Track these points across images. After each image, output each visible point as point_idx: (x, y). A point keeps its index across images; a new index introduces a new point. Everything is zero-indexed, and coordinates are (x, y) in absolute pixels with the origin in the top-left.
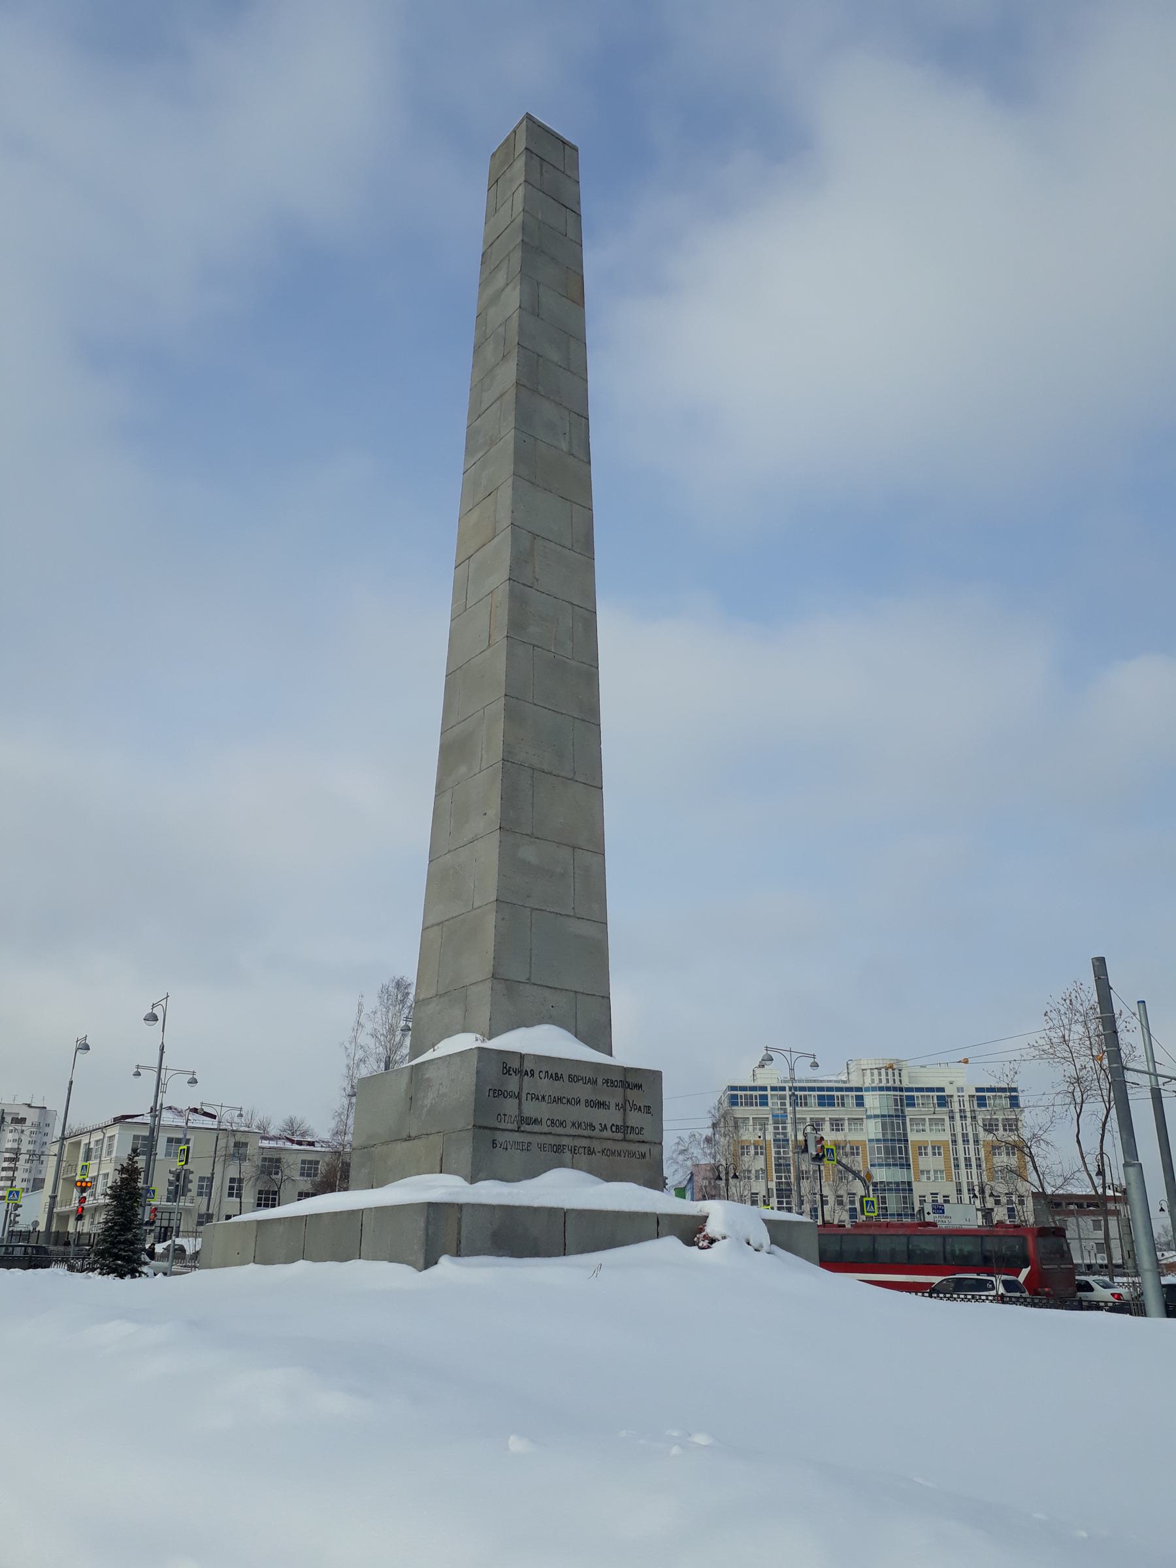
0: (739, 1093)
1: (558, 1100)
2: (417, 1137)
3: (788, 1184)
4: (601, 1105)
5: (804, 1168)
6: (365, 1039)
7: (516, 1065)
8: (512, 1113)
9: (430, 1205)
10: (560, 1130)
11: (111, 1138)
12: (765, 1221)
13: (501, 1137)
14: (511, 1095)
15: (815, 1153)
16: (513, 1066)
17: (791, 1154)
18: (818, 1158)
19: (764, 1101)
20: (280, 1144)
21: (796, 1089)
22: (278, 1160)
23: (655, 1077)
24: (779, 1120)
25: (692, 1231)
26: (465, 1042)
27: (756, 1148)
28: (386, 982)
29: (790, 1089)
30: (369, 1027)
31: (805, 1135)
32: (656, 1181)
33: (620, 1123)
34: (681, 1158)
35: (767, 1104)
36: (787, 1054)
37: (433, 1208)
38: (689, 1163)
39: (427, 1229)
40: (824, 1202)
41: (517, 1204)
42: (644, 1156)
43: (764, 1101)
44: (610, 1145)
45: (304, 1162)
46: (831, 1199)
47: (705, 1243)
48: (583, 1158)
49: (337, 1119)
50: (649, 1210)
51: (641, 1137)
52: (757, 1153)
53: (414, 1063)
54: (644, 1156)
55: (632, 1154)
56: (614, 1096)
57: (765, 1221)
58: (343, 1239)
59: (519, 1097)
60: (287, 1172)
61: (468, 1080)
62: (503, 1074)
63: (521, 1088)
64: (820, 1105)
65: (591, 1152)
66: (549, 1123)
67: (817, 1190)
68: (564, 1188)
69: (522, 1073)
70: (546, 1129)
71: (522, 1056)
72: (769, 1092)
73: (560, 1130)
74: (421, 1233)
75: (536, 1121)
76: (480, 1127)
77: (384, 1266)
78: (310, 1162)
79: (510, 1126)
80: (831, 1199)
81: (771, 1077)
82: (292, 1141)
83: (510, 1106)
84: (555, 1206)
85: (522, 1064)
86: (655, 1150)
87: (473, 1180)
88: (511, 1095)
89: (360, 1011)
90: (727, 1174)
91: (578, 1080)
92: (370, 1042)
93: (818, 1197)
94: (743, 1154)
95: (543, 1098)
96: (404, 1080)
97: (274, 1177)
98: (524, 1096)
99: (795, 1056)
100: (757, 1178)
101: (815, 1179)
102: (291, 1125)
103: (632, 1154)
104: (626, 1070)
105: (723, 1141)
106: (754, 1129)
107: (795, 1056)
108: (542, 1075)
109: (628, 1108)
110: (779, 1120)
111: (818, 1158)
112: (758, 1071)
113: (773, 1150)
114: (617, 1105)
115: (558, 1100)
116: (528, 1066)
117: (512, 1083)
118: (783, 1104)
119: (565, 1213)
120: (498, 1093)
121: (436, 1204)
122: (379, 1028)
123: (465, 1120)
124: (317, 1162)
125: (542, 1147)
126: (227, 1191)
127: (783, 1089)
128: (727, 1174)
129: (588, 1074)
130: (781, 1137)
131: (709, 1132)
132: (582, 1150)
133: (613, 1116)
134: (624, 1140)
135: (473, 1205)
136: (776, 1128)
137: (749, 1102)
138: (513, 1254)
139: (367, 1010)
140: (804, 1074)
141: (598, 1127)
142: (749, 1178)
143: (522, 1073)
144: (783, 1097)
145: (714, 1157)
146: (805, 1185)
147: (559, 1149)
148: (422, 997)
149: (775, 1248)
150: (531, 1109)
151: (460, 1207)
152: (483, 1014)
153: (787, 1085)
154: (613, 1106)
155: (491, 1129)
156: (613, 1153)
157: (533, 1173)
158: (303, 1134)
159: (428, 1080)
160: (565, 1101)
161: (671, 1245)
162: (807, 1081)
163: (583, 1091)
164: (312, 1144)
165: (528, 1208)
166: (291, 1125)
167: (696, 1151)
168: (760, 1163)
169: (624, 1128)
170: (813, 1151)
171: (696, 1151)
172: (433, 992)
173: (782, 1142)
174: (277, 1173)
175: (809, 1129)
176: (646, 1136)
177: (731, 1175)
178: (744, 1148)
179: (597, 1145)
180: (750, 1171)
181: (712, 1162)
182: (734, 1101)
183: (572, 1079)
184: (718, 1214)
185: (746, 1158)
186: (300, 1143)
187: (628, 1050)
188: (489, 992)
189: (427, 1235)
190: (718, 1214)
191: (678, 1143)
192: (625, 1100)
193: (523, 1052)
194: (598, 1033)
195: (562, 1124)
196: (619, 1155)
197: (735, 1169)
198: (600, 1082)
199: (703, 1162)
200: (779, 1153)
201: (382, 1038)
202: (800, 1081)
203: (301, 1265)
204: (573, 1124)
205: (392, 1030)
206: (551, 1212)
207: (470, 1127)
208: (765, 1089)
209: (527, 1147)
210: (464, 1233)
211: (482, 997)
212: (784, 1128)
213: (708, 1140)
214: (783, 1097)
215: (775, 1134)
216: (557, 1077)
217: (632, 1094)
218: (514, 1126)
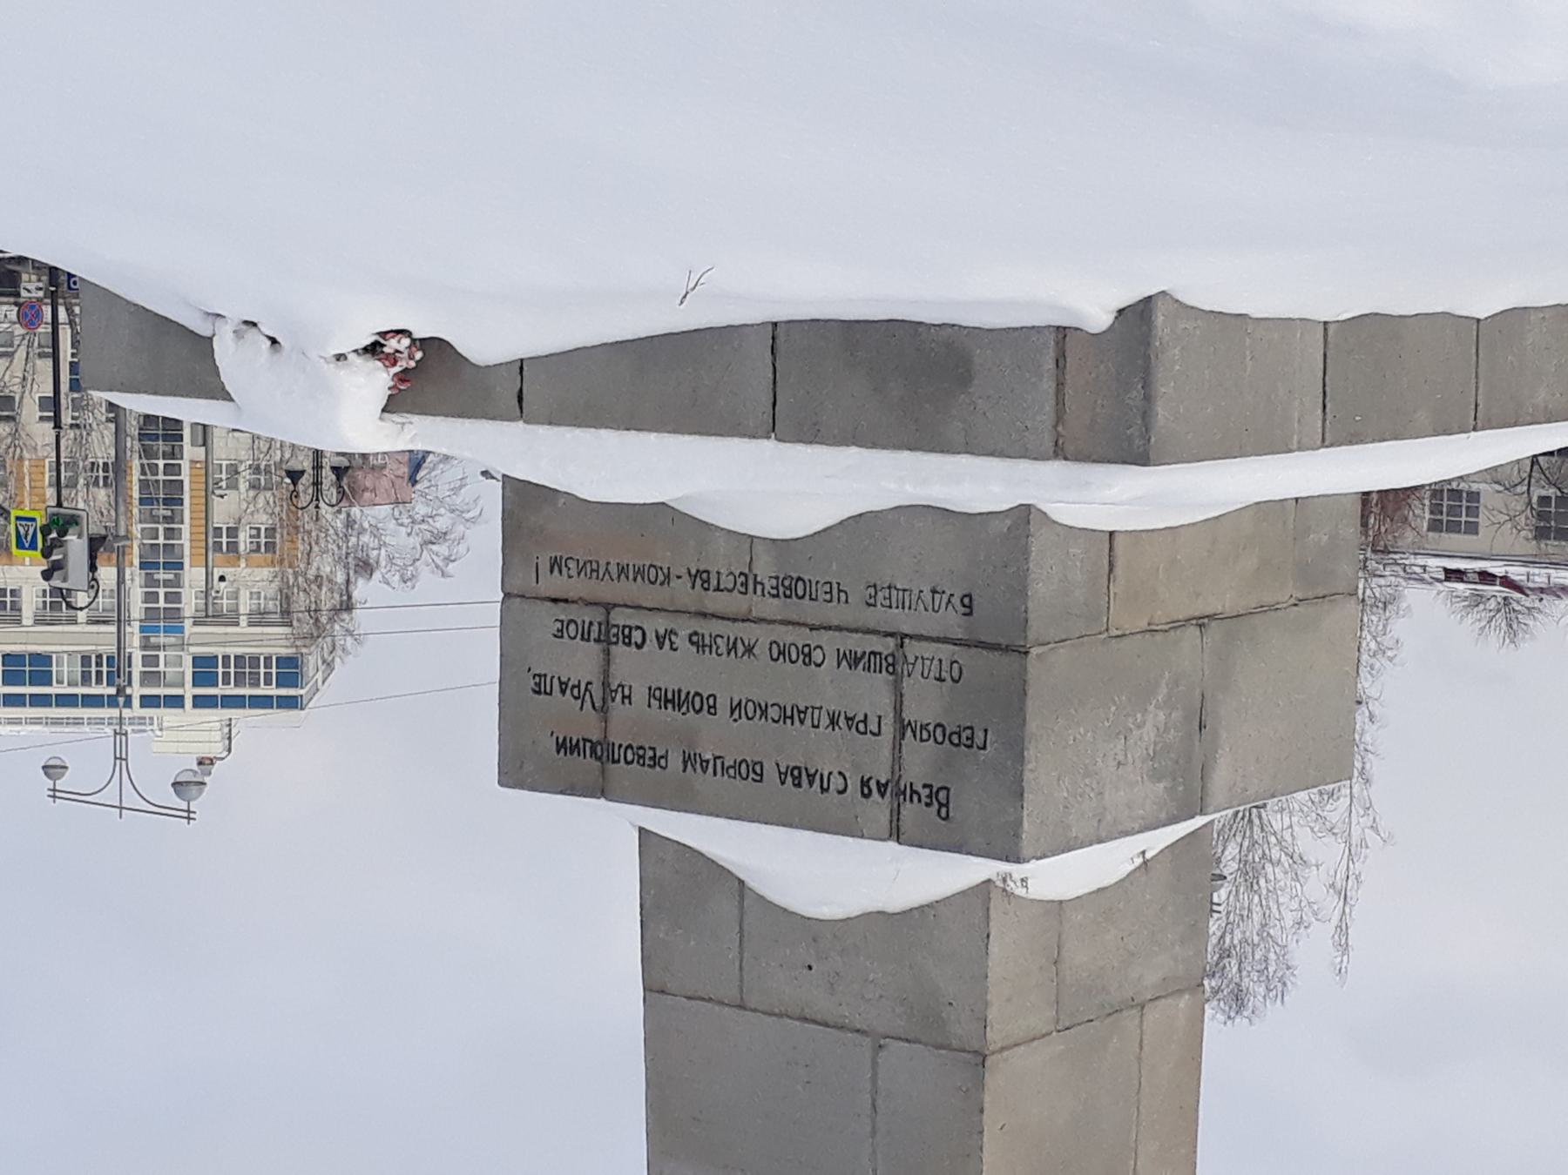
0: (273, 691)
1: (793, 715)
2: (1178, 625)
3: (147, 453)
4: (672, 700)
5: (102, 494)
6: (1324, 853)
7: (909, 810)
8: (927, 686)
9: (1143, 459)
10: (788, 635)
12: (228, 397)
13: (951, 621)
14: (923, 732)
15: (71, 537)
16: (917, 808)
17: (136, 529)
18: (62, 523)
19: (205, 670)
20: (1540, 576)
21: (112, 702)
22: (1541, 534)
23: (517, 771)
24: (163, 619)
25: (427, 374)
26: (1056, 877)
27: (233, 547)
28: (1273, 1010)
29: (129, 699)
30: (1315, 886)
31: (93, 583)
32: (525, 504)
33: (619, 650)
34: (441, 524)
35: (196, 660)
36: (131, 799)
37: (1136, 451)
38: (421, 509)
39: (1148, 398)
40: (53, 404)
41: (906, 455)
42: (555, 564)
43: (205, 670)
44: (651, 595)
45: (1473, 529)
46: (30, 412)
47: (392, 345)
48: (722, 563)
49: (1387, 641)
50: (542, 430)
51: (562, 612)
52: (233, 532)
53: (1199, 821)
54: (555, 564)
55: (589, 569)
56: (633, 720)
57: (228, 397)
58: (1370, 370)
59: (902, 727)
60: (1518, 505)
61: (1045, 777)
62: (952, 779)
63: (897, 747)
64: (45, 659)
65: (701, 578)
66: (817, 656)
67: (68, 436)
68: (776, 490)
69: (895, 790)
70: (824, 638)
71: (896, 833)
72: (189, 691)
73: (788, 635)
74: (1165, 388)
75: (854, 660)
76: (1007, 649)
77: (1258, 306)
78: (1454, 527)
79: (927, 649)
80: (30, 412)
81: (185, 733)
82: (1507, 582)
83: (925, 703)
84: (800, 448)
85: (896, 814)
86: (520, 582)
87: (1024, 514)
88: (923, 732)
89: (1342, 929)
90: (317, 484)
91: (737, 766)
92: (1305, 841)
93: (66, 419)
94: (271, 531)
95: (833, 722)
96: (1221, 777)
97: (1551, 492)
98: (888, 728)
99: (110, 795)
100: (234, 471)
101: (73, 465)
102: (1512, 623)
103: (589, 569)
104: (601, 790)
105: (325, 565)
106: (235, 595)
108: (837, 782)
109: (597, 691)
110: (163, 619)
111: (62, 523)
112: (217, 749)
113: (185, 540)
114: (627, 698)
115: (793, 715)
116: (879, 808)
117: (920, 763)
118: (150, 661)
119: (772, 428)
120: (961, 738)
121: (1125, 462)
122: (1284, 880)
123: (1048, 670)
124: (1435, 526)
125: (836, 593)
127: (147, 701)
128: (317, 484)
129: (704, 782)
130: (162, 575)
131: (362, 589)
132: (727, 582)
133: (636, 668)
134: (609, 607)
135: (1025, 454)
136: (174, 597)
137: (246, 667)
138: (915, 328)
139: (1321, 934)
140: (83, 742)
141: (681, 641)
142: (256, 469)
143: (895, 790)
144: (149, 678)
145: (350, 523)
146: (101, 447)
147: (789, 587)
148: (1184, 1001)
149: (203, 329)
150: (869, 694)
151: (1059, 452)
152: (1006, 952)
153: (137, 710)
154: (640, 695)
155: (981, 645)
156: (639, 572)
157: (861, 529)
158: (1478, 600)
159: (1156, 776)
160: (773, 713)
161: (486, 342)
162: (78, 722)
163: (717, 735)
164: (1453, 575)
165: (874, 445)
166: (1512, 623)
167: (399, 539)
168: (224, 510)
169: (608, 637)
170: (76, 545)
171: (399, 539)
172: (1153, 1015)
173: (162, 562)
174: (1544, 500)
175: (82, 599)
176: (548, 617)
177: (306, 480)
178: (267, 545)
179: (683, 592)
180: (254, 486)
181: (355, 511)
182: (290, 671)
183: (755, 771)
184: (356, 416)
185: (263, 520)
186: (1486, 577)
187: (598, 841)
188: (992, 1014)
189: (1146, 384)
190: (356, 416)
191: (448, 560)
192: (603, 710)
193: (892, 845)
194: (678, 892)
195: (781, 653)
196: (623, 570)
197: (294, 494)
198: (675, 761)
199: (384, 510)
200: (170, 533)
201: (1275, 853)
202: (100, 721)
203: (1482, 306)
204: (749, 650)
205: (1250, 874)
206: (811, 432)
207: (1034, 651)
208: (200, 702)
209: (875, 593)
210: (1048, 385)
211: (1012, 1003)
212: (150, 597)
213: (366, 567)
214: (149, 678)
215: (177, 583)
216: (796, 776)
217: (586, 725)
218: (913, 649)
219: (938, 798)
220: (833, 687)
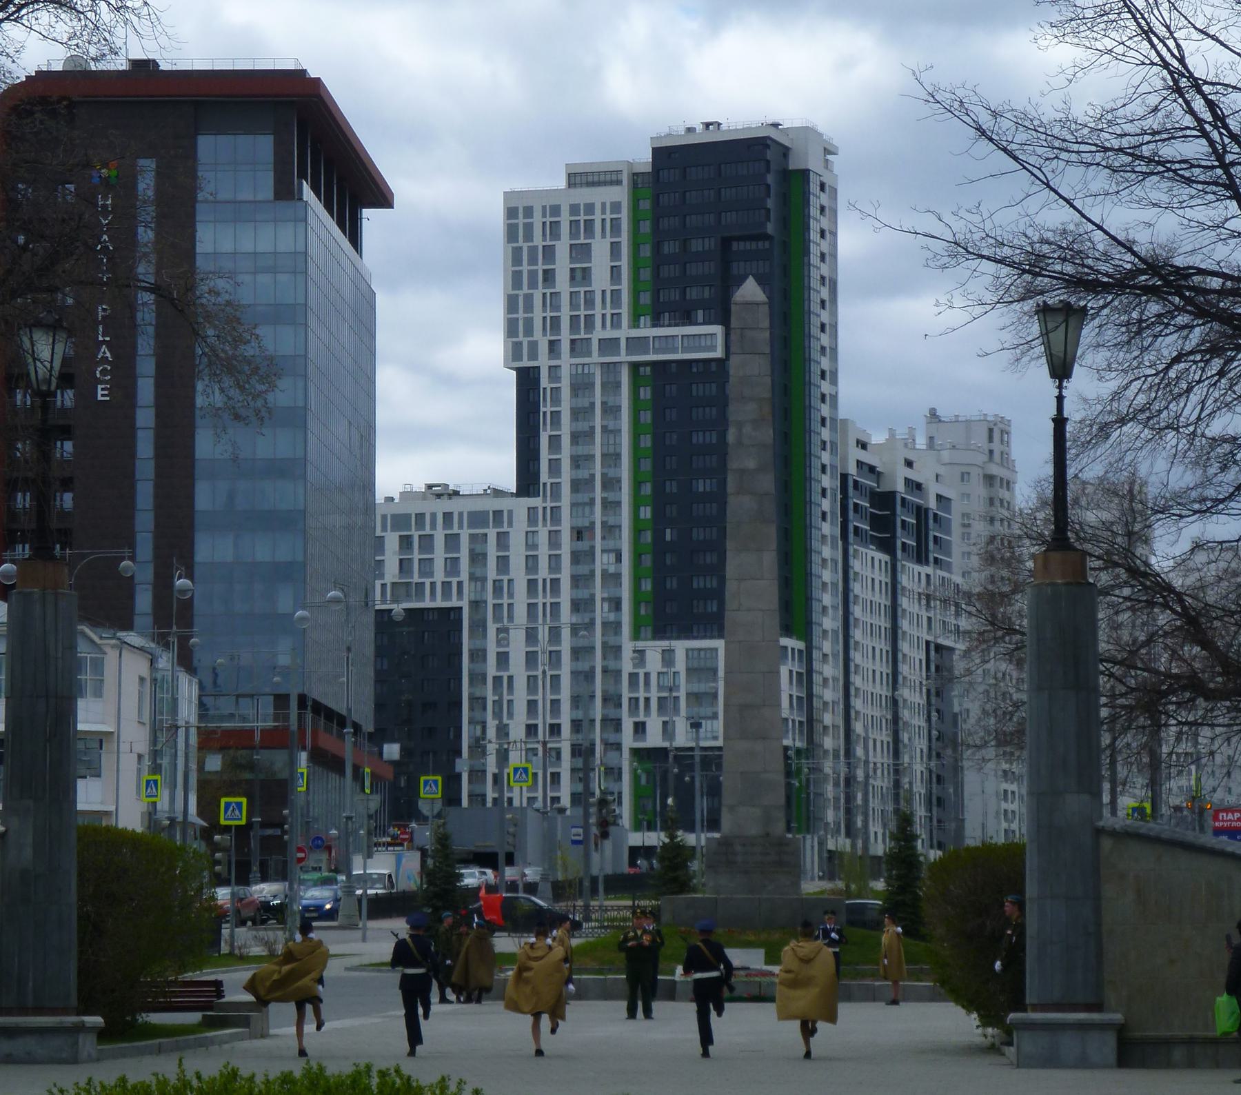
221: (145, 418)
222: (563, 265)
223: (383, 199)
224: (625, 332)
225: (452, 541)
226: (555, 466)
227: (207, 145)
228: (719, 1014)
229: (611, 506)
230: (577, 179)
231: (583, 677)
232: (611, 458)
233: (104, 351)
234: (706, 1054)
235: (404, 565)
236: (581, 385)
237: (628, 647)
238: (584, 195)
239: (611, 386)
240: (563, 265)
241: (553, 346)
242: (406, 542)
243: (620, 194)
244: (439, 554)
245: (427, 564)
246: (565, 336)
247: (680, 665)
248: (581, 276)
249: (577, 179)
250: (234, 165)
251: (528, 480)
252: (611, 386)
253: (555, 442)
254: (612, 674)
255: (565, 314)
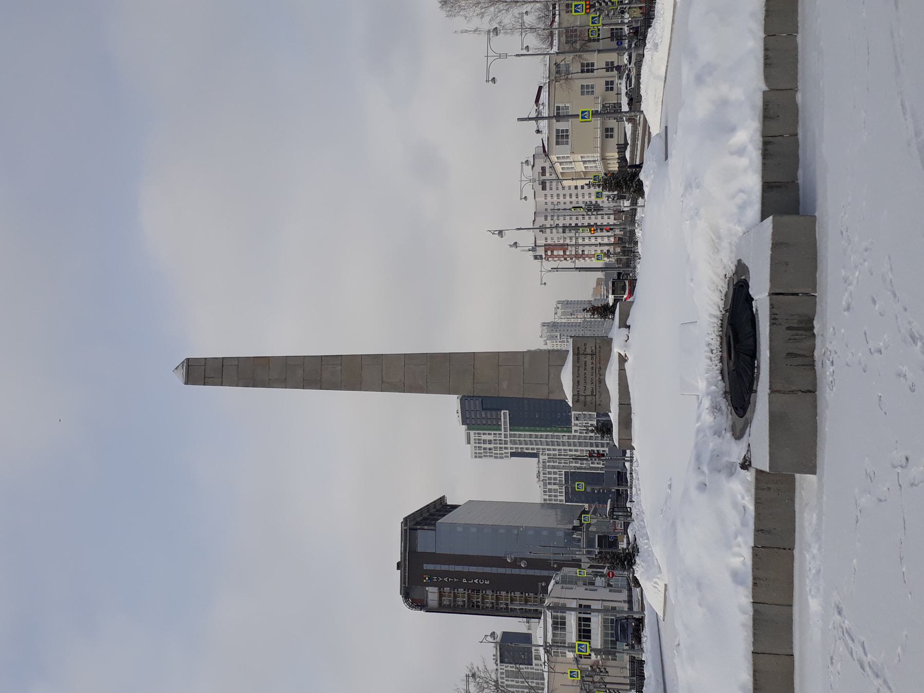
11: (558, 158)
36: (490, 60)
83: (589, 399)
89: (467, 31)
99: (491, 53)
107: (491, 53)
117: (582, 398)
126: (590, 74)
150: (588, 392)
161: (627, 366)
179: (598, 366)
186: (554, 15)
219: (578, 401)
220: (589, 386)
221: (494, 570)
222: (488, 446)
223: (443, 499)
224: (503, 432)
225: (549, 473)
226: (533, 449)
227: (419, 550)
228: (741, 268)
229: (541, 437)
230: (469, 443)
231: (580, 444)
232: (531, 436)
233: (476, 581)
234: (200, 372)
235: (555, 484)
236: (514, 443)
237: (573, 433)
238: (472, 441)
239: (515, 436)
240: (488, 446)
241: (506, 448)
242: (550, 484)
243: (472, 433)
244: (553, 476)
245: (555, 479)
246: (503, 446)
247: (577, 422)
248: (490, 442)
249: (469, 443)
250: (426, 541)
251: (535, 455)
252: (515, 436)
253: (527, 449)
254: (579, 438)
255: (499, 446)
